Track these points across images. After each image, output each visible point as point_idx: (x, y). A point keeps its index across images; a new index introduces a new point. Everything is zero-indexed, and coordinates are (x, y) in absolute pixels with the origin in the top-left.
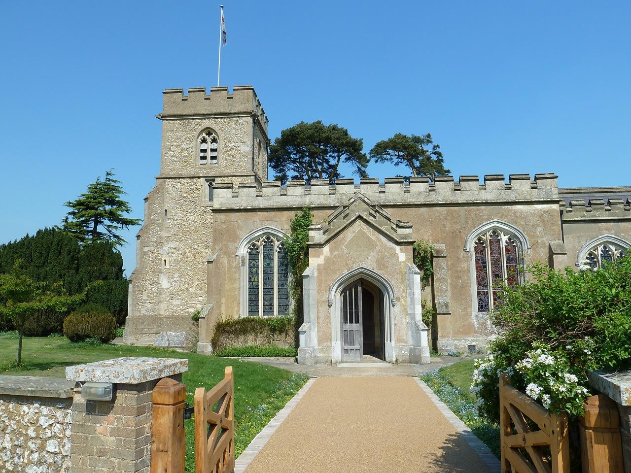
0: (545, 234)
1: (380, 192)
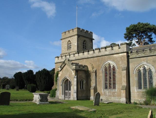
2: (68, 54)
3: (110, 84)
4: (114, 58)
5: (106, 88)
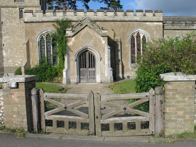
1: (95, 15)
4: (146, 26)
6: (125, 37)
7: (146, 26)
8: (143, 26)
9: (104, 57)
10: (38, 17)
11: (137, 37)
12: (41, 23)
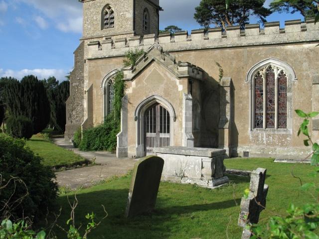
0: (309, 68)
1: (187, 41)
2: (104, 39)
3: (269, 117)
4: (286, 52)
5: (257, 124)
6: (242, 77)
7: (286, 52)
8: (278, 53)
9: (181, 114)
10: (105, 51)
11: (267, 75)
12: (108, 60)
